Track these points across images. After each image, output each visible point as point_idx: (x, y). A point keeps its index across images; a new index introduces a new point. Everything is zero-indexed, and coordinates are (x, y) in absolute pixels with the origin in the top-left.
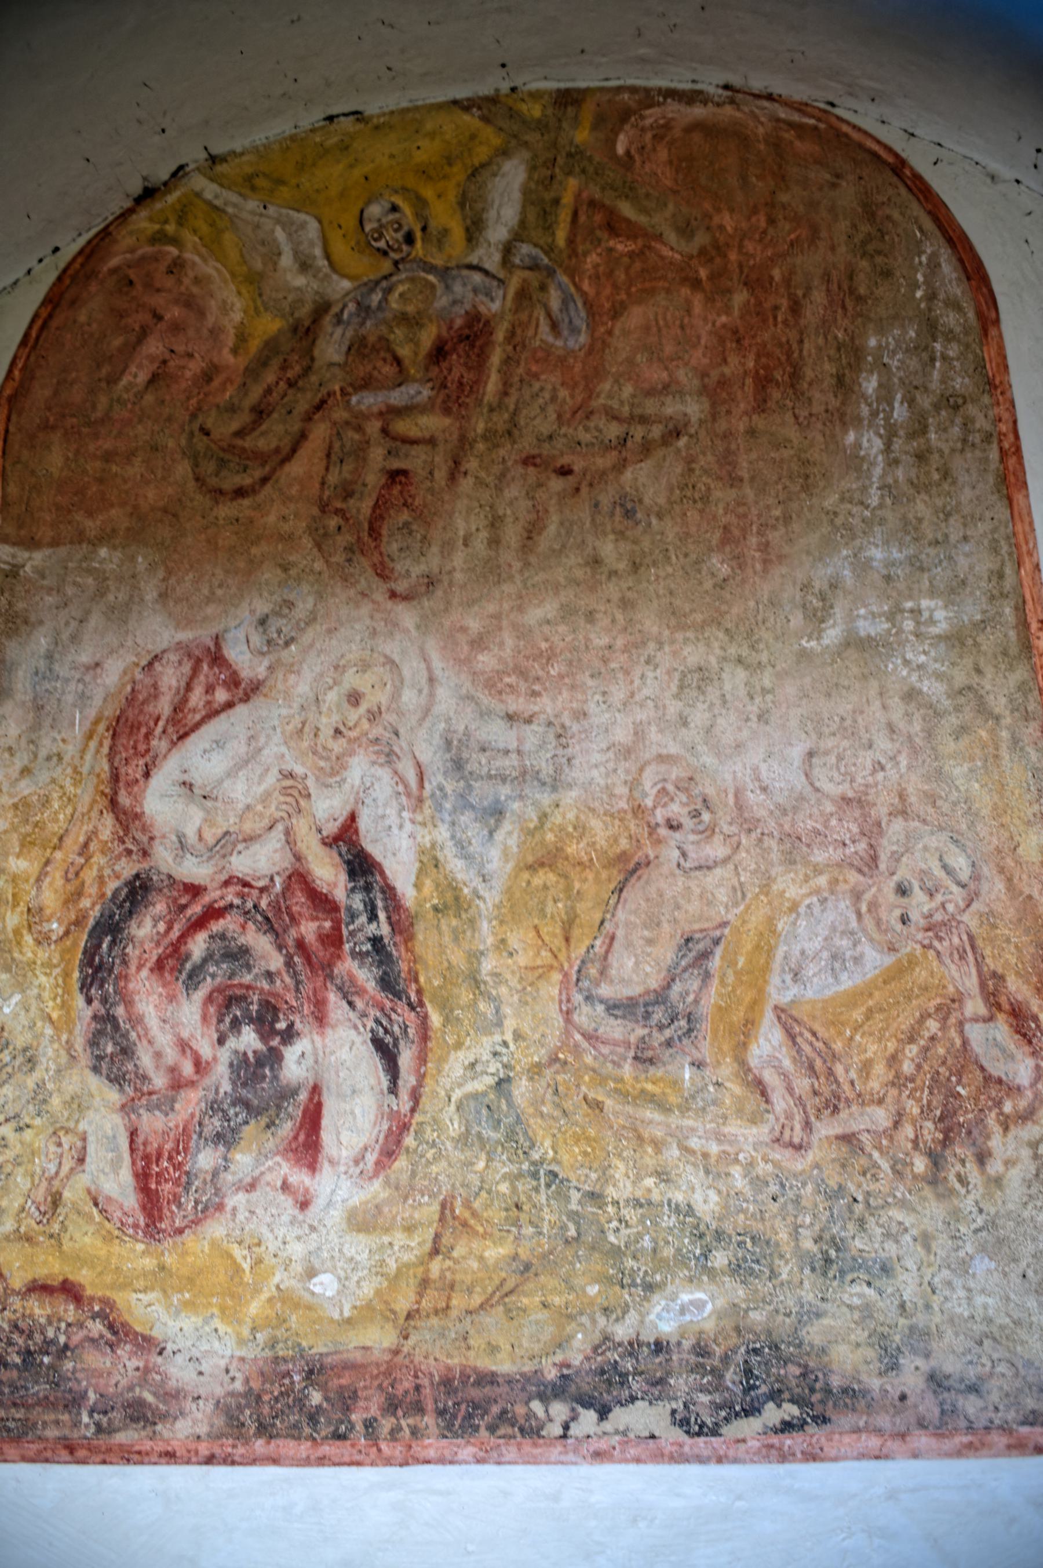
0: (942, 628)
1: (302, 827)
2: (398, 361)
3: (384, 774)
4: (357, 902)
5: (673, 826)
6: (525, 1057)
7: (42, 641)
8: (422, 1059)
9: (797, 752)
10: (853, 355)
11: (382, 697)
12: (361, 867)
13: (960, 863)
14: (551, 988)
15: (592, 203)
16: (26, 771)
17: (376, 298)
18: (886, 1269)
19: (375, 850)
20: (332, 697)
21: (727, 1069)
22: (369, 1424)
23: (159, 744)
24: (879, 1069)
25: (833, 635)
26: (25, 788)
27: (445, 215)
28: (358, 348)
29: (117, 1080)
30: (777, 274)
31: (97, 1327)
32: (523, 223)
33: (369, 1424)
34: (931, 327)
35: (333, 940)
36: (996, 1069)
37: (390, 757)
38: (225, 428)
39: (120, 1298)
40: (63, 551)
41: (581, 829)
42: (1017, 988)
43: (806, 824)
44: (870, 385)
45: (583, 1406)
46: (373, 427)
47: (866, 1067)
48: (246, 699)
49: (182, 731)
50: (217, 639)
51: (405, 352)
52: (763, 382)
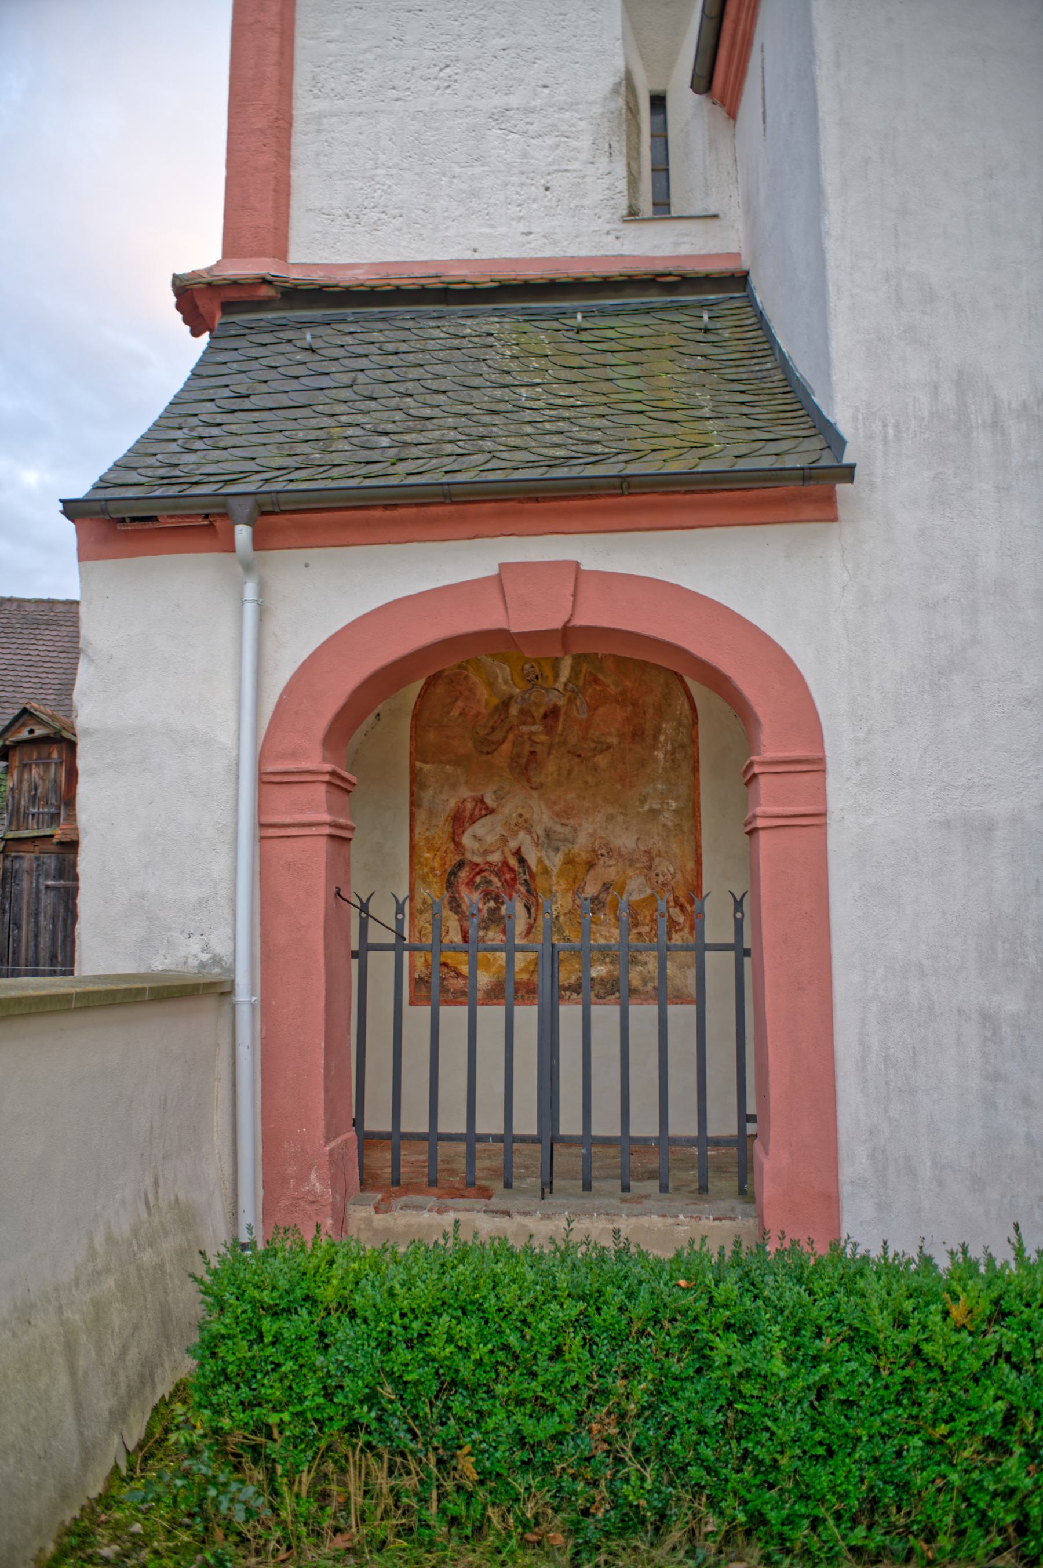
0: (674, 808)
1: (506, 849)
2: (533, 717)
3: (528, 837)
4: (521, 870)
5: (602, 855)
6: (563, 911)
7: (430, 792)
8: (537, 910)
9: (635, 838)
10: (658, 731)
11: (528, 816)
12: (522, 861)
13: (672, 869)
14: (570, 895)
15: (591, 673)
16: (428, 829)
17: (527, 696)
18: (646, 963)
19: (526, 857)
20: (515, 815)
21: (612, 916)
22: (522, 996)
23: (466, 824)
24: (648, 917)
25: (646, 807)
26: (428, 834)
27: (548, 672)
28: (522, 712)
29: (457, 913)
30: (640, 702)
31: (453, 974)
32: (570, 677)
33: (522, 996)
34: (680, 724)
35: (514, 879)
36: (676, 919)
37: (530, 832)
38: (483, 732)
39: (459, 967)
40: (435, 765)
41: (579, 855)
42: (682, 900)
43: (635, 857)
44: (662, 738)
45: (812, 1522)
46: (526, 737)
47: (645, 917)
48: (491, 813)
49: (473, 821)
50: (482, 796)
51: (535, 714)
52: (634, 735)
